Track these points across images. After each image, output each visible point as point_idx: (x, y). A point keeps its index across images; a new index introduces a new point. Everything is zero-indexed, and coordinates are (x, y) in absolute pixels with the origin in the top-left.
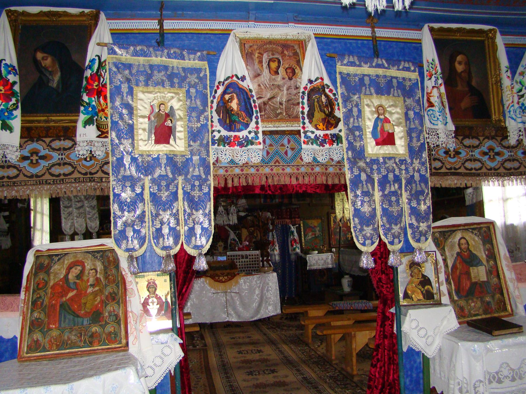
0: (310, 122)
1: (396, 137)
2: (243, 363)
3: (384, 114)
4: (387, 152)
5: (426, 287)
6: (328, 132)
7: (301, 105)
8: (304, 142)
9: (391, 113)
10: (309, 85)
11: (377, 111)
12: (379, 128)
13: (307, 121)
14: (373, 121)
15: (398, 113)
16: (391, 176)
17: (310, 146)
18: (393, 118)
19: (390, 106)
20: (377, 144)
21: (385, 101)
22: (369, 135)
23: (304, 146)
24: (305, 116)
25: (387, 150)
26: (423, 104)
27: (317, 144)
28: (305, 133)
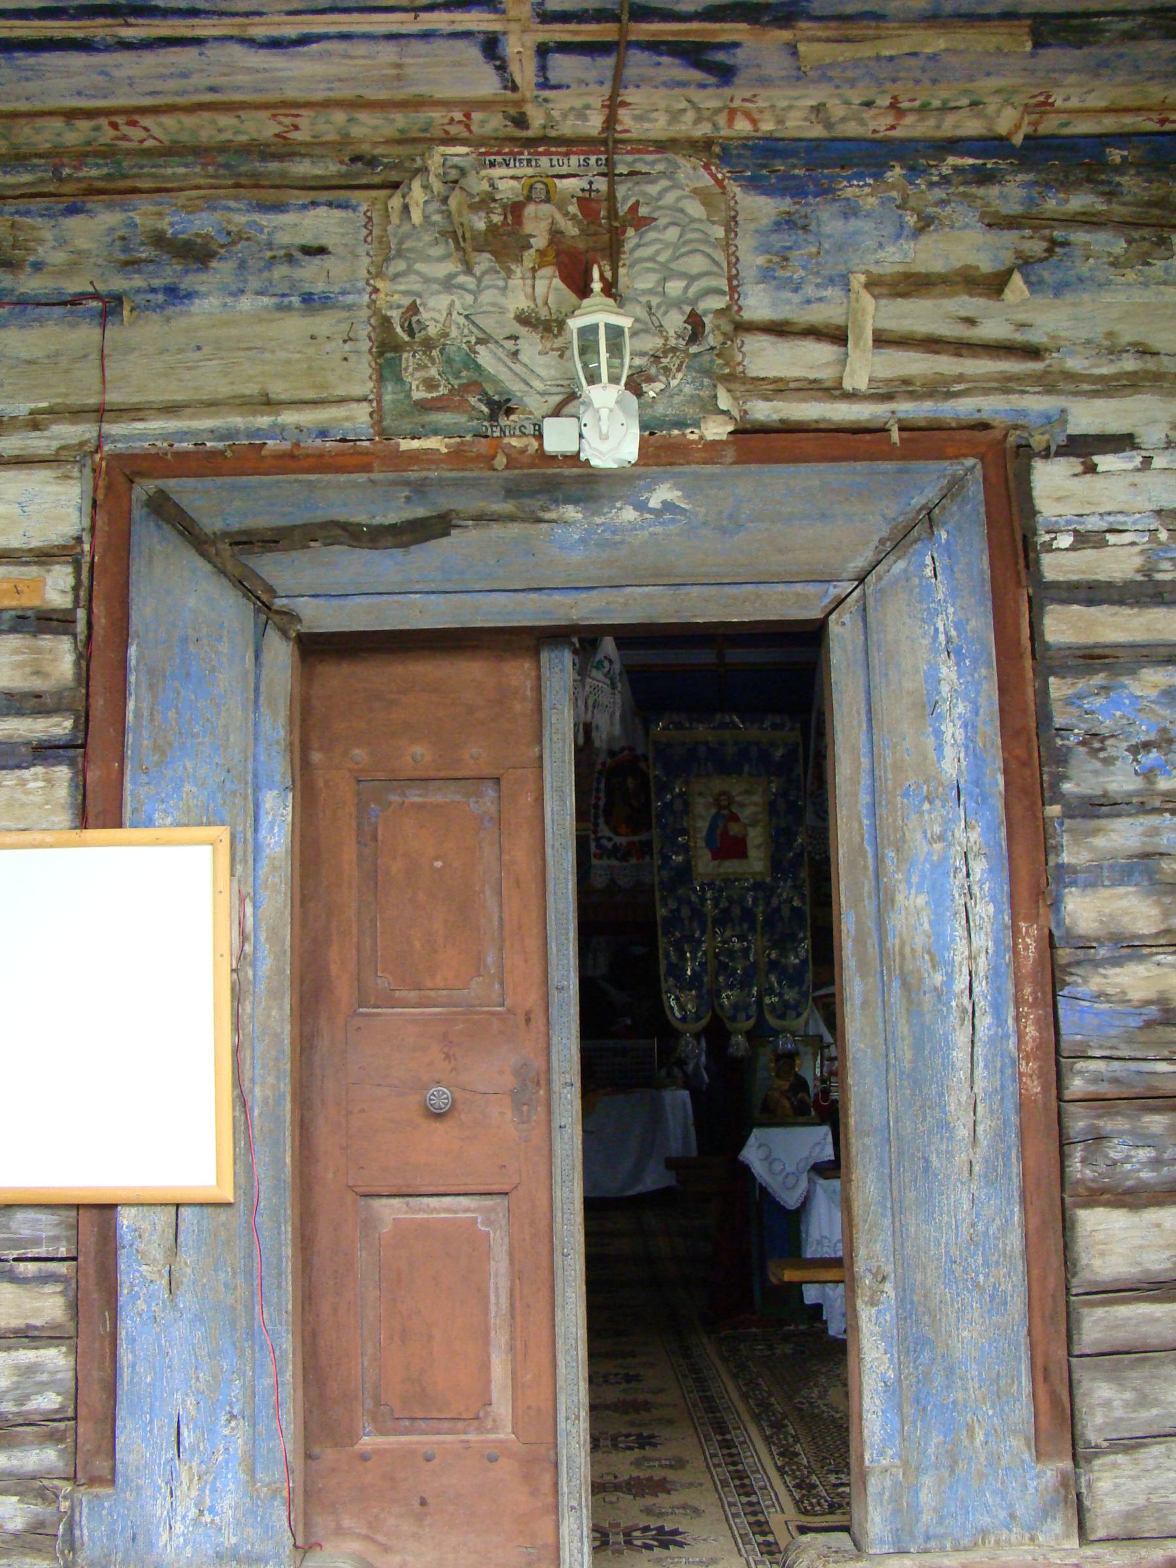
0: (607, 822)
1: (749, 842)
2: (646, 1403)
3: (728, 807)
4: (730, 870)
5: (800, 1095)
6: (635, 838)
7: (594, 794)
8: (595, 856)
9: (742, 806)
10: (609, 761)
11: (717, 802)
12: (718, 831)
13: (601, 820)
14: (709, 819)
15: (756, 805)
16: (736, 911)
17: (605, 862)
18: (745, 814)
19: (741, 794)
20: (714, 858)
21: (734, 786)
22: (701, 843)
23: (594, 861)
24: (600, 812)
25: (731, 866)
26: (805, 786)
27: (617, 859)
28: (597, 840)
